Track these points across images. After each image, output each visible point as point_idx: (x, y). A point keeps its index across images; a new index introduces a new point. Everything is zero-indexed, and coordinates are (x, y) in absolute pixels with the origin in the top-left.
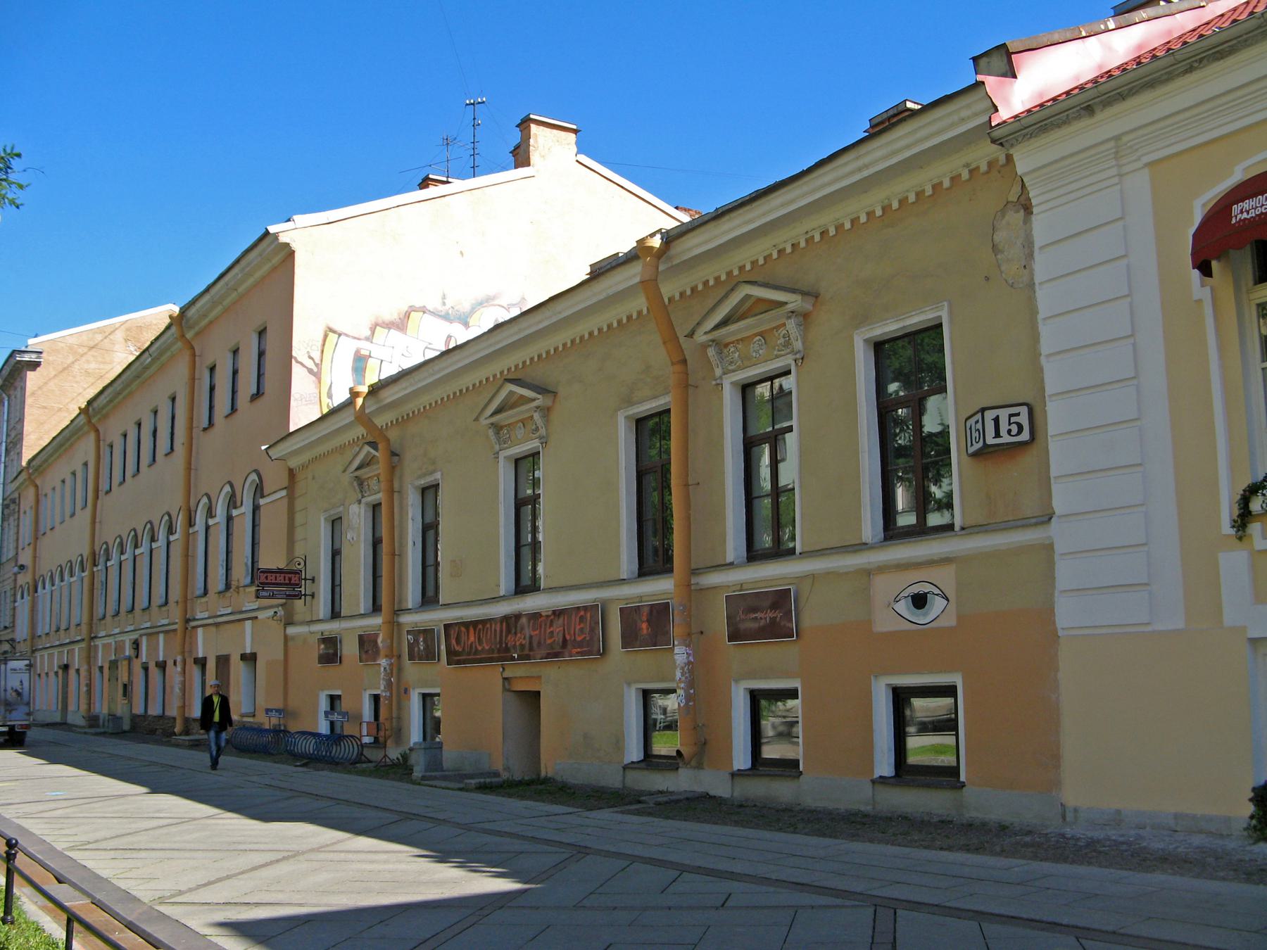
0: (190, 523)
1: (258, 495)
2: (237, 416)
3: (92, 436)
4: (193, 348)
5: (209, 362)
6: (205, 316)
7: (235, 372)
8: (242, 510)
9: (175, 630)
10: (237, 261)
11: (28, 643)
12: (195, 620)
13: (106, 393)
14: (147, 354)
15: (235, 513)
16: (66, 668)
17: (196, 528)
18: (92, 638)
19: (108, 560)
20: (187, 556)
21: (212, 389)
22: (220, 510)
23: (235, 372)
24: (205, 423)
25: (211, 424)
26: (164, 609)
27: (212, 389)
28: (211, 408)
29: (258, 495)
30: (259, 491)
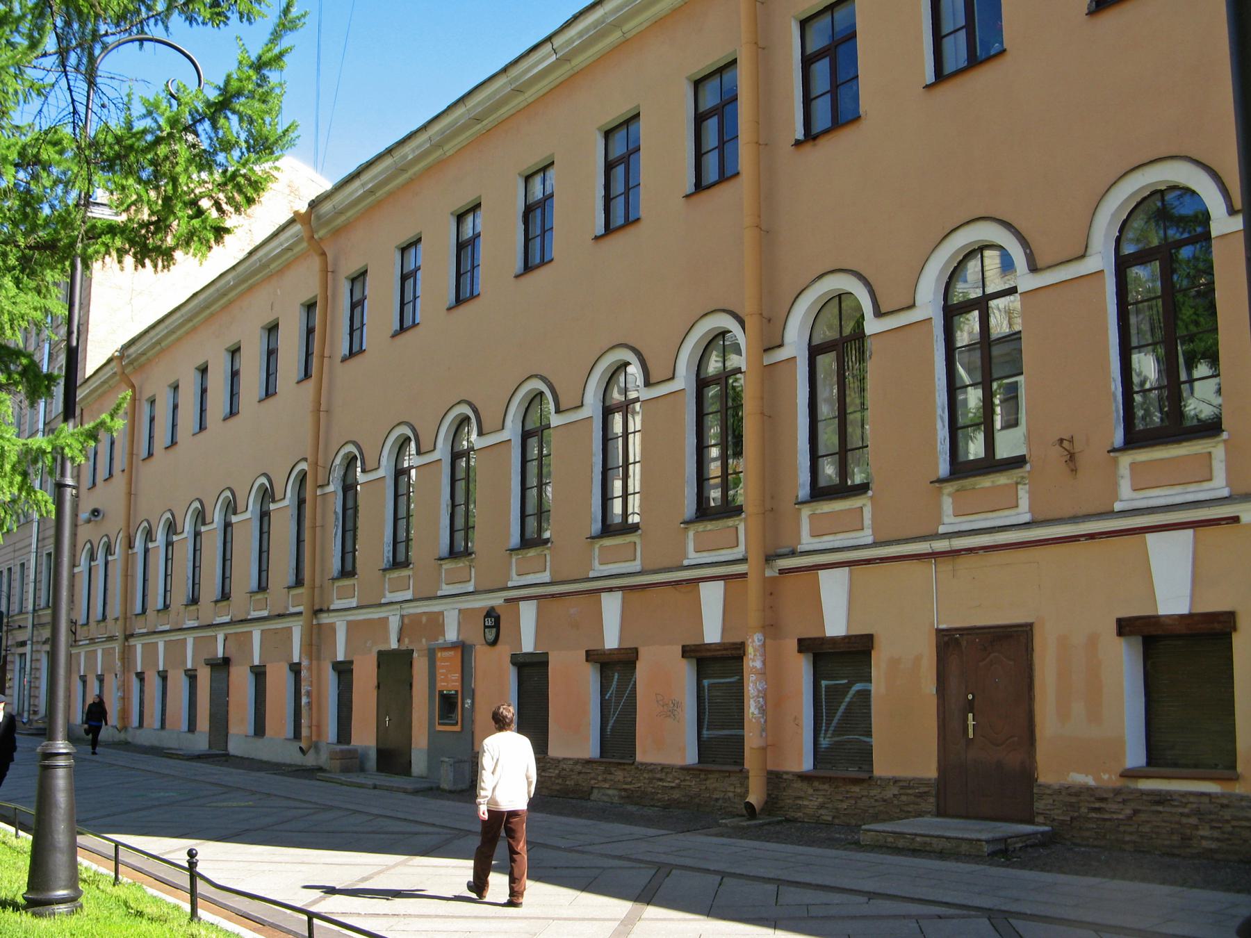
0: (130, 545)
1: (230, 511)
2: (177, 449)
3: (315, 263)
4: (324, 254)
5: (353, 267)
6: (341, 213)
7: (175, 407)
8: (156, 544)
9: (743, 576)
10: (504, 70)
11: (120, 623)
12: (793, 553)
13: (365, 177)
14: (547, 48)
15: (151, 545)
16: (221, 666)
17: (135, 550)
18: (317, 612)
19: (74, 566)
20: (126, 576)
21: (152, 419)
22: (217, 517)
23: (175, 407)
24: (144, 454)
25: (150, 455)
26: (102, 624)
27: (152, 419)
28: (151, 437)
29: (230, 511)
30: (171, 528)
